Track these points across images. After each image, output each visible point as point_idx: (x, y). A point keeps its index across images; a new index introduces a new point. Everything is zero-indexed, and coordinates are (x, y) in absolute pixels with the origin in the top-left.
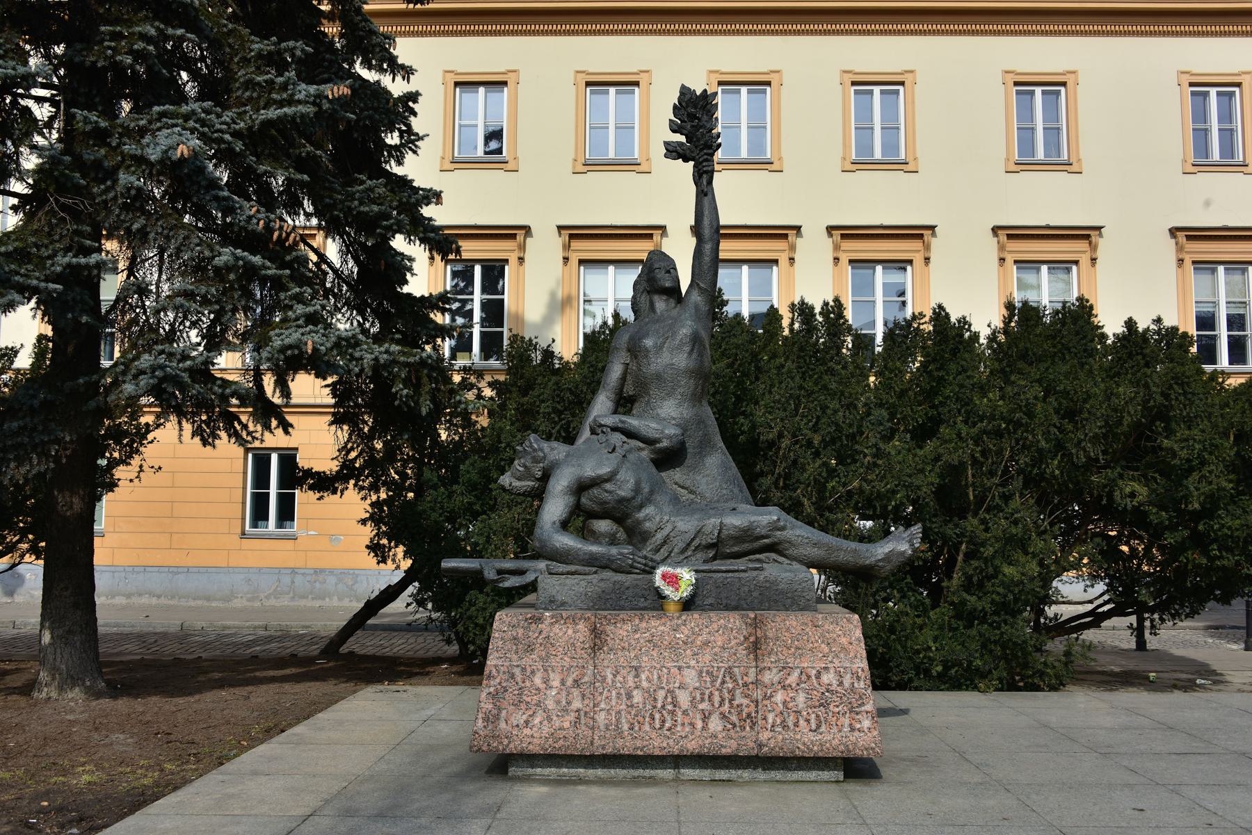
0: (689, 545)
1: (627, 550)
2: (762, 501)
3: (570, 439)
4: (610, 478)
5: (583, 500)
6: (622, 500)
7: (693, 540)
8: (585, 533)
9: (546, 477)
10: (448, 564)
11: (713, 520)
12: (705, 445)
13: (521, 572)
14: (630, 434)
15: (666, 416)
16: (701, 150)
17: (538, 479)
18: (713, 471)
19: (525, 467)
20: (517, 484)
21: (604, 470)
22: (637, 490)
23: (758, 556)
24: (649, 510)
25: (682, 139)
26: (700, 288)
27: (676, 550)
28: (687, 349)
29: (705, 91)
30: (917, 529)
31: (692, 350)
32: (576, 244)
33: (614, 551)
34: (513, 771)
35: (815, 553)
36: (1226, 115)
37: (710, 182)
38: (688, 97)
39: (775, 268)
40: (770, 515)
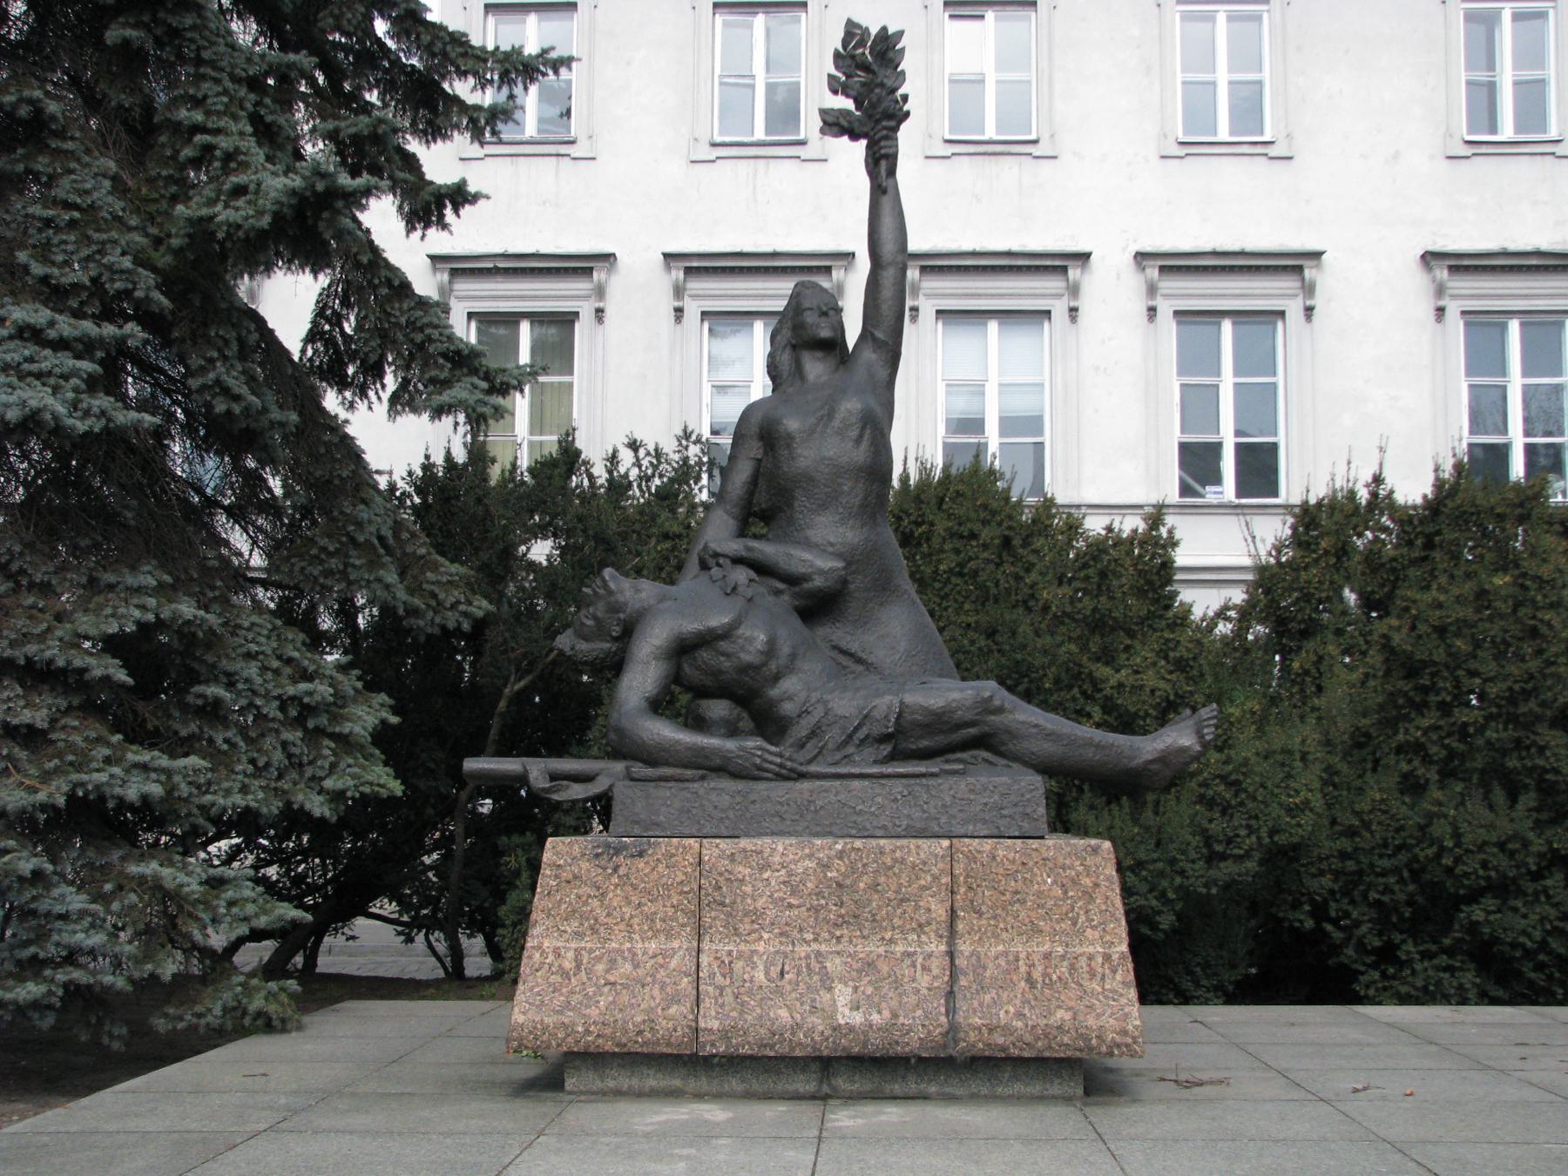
0: (850, 737)
1: (753, 743)
2: (966, 672)
4: (726, 634)
5: (686, 667)
6: (746, 668)
7: (856, 729)
8: (698, 723)
9: (628, 632)
10: (471, 764)
11: (887, 699)
12: (883, 587)
14: (762, 569)
17: (616, 639)
19: (595, 618)
20: (583, 646)
21: (718, 620)
22: (770, 650)
23: (959, 755)
24: (789, 684)
25: (848, 104)
27: (830, 746)
28: (854, 433)
29: (884, 29)
31: (861, 436)
32: (696, 285)
33: (730, 745)
34: (570, 1083)
35: (1044, 748)
36: (1531, 54)
37: (892, 172)
39: (1046, 324)
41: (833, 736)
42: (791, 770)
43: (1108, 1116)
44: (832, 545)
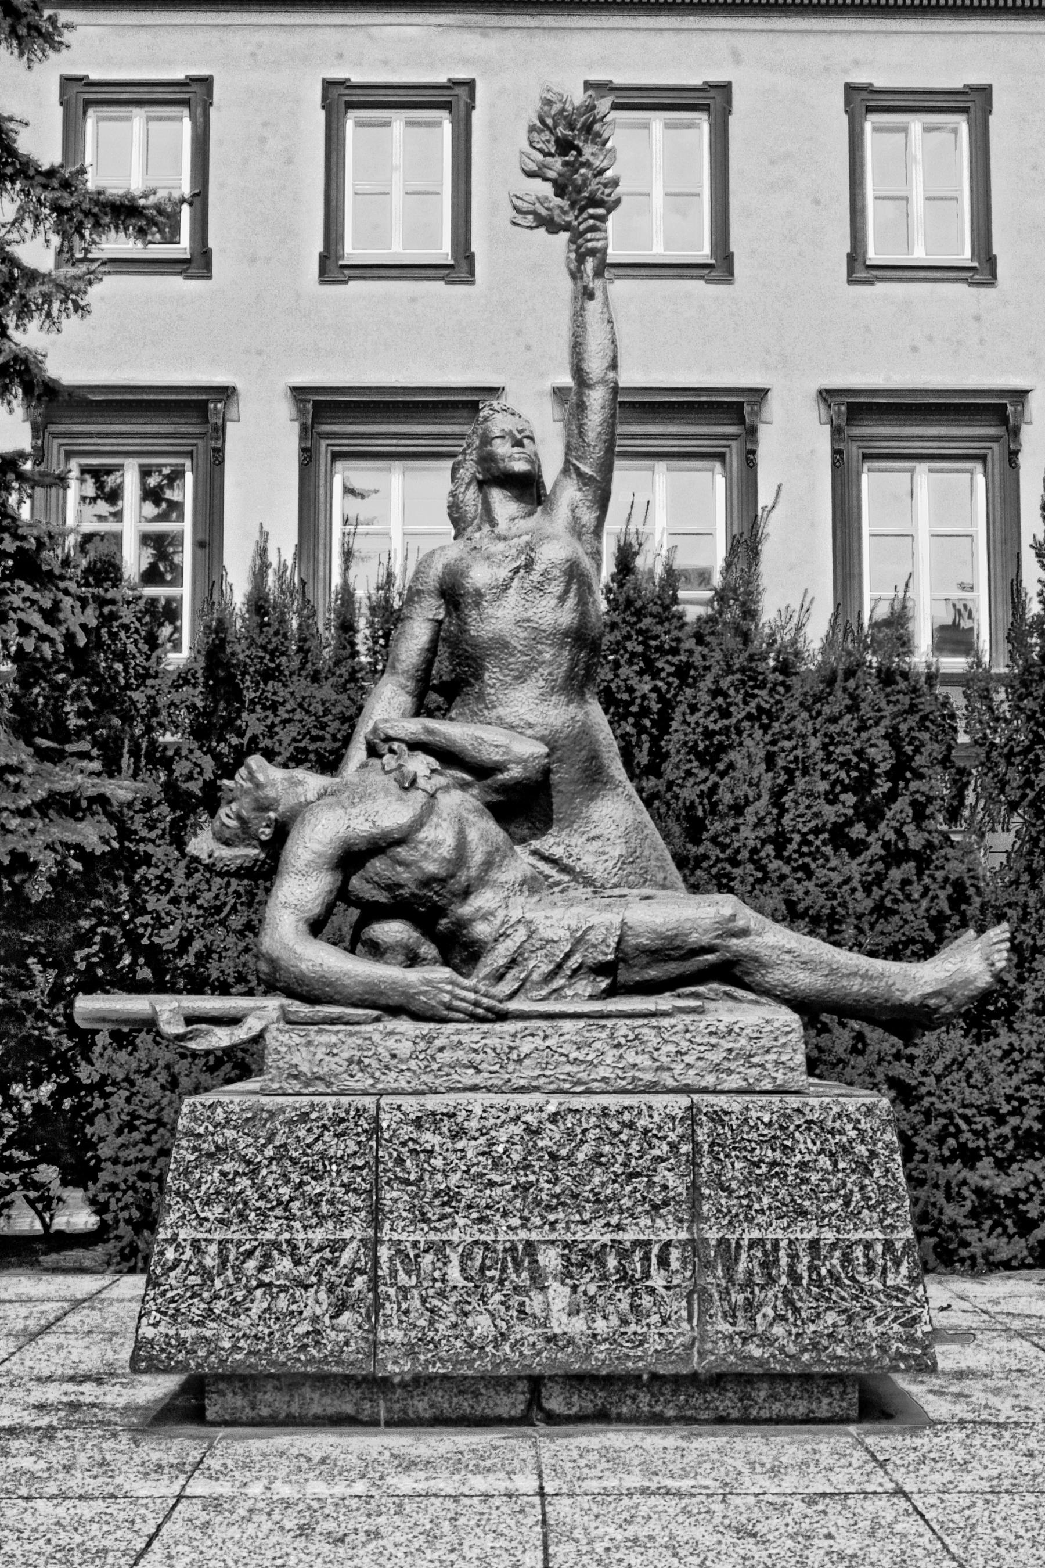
0: (559, 966)
3: (329, 764)
6: (428, 882)
7: (568, 956)
8: (357, 942)
9: (282, 831)
13: (233, 1021)
14: (448, 757)
15: (520, 721)
16: (582, 210)
18: (612, 821)
20: (224, 852)
24: (483, 900)
26: (580, 474)
30: (1000, 932)
31: (566, 592)
33: (413, 976)
35: (804, 980)
38: (556, 107)
40: (721, 906)
41: (539, 965)
42: (488, 1009)
43: (884, 1441)
44: (531, 726)
